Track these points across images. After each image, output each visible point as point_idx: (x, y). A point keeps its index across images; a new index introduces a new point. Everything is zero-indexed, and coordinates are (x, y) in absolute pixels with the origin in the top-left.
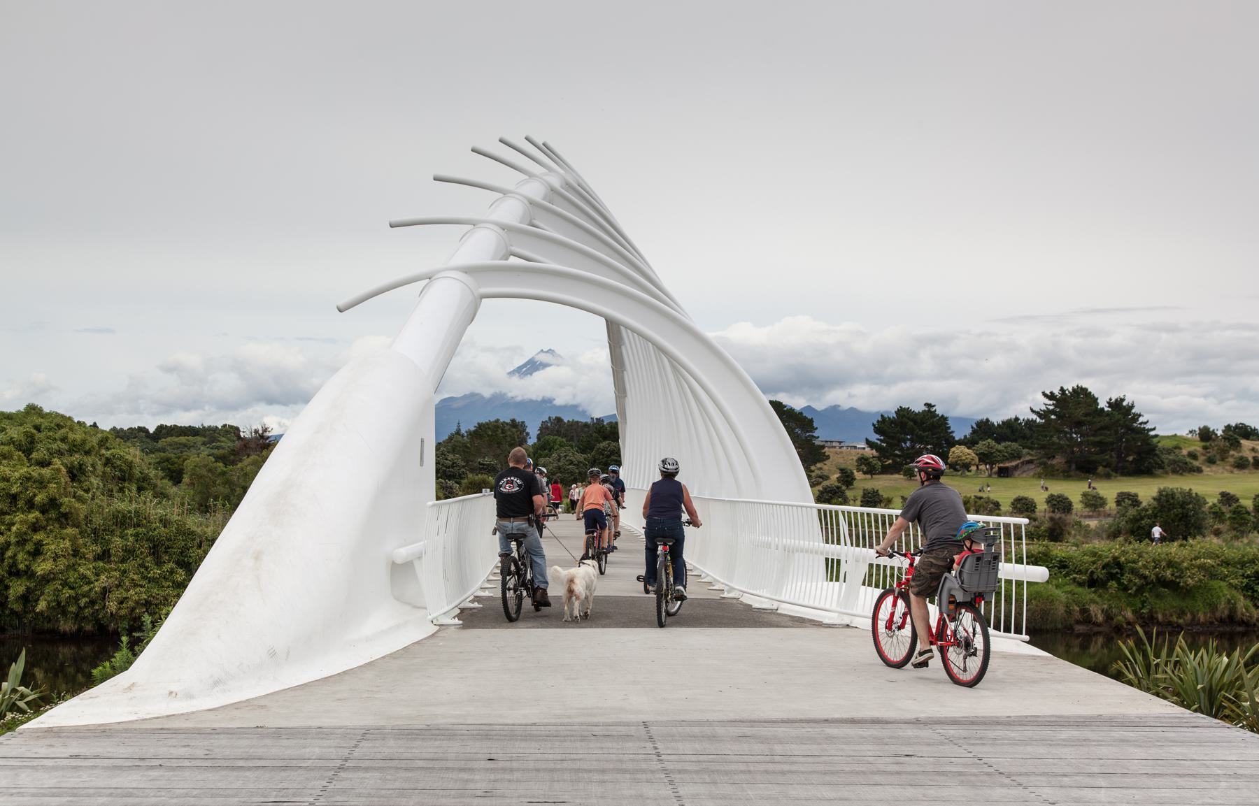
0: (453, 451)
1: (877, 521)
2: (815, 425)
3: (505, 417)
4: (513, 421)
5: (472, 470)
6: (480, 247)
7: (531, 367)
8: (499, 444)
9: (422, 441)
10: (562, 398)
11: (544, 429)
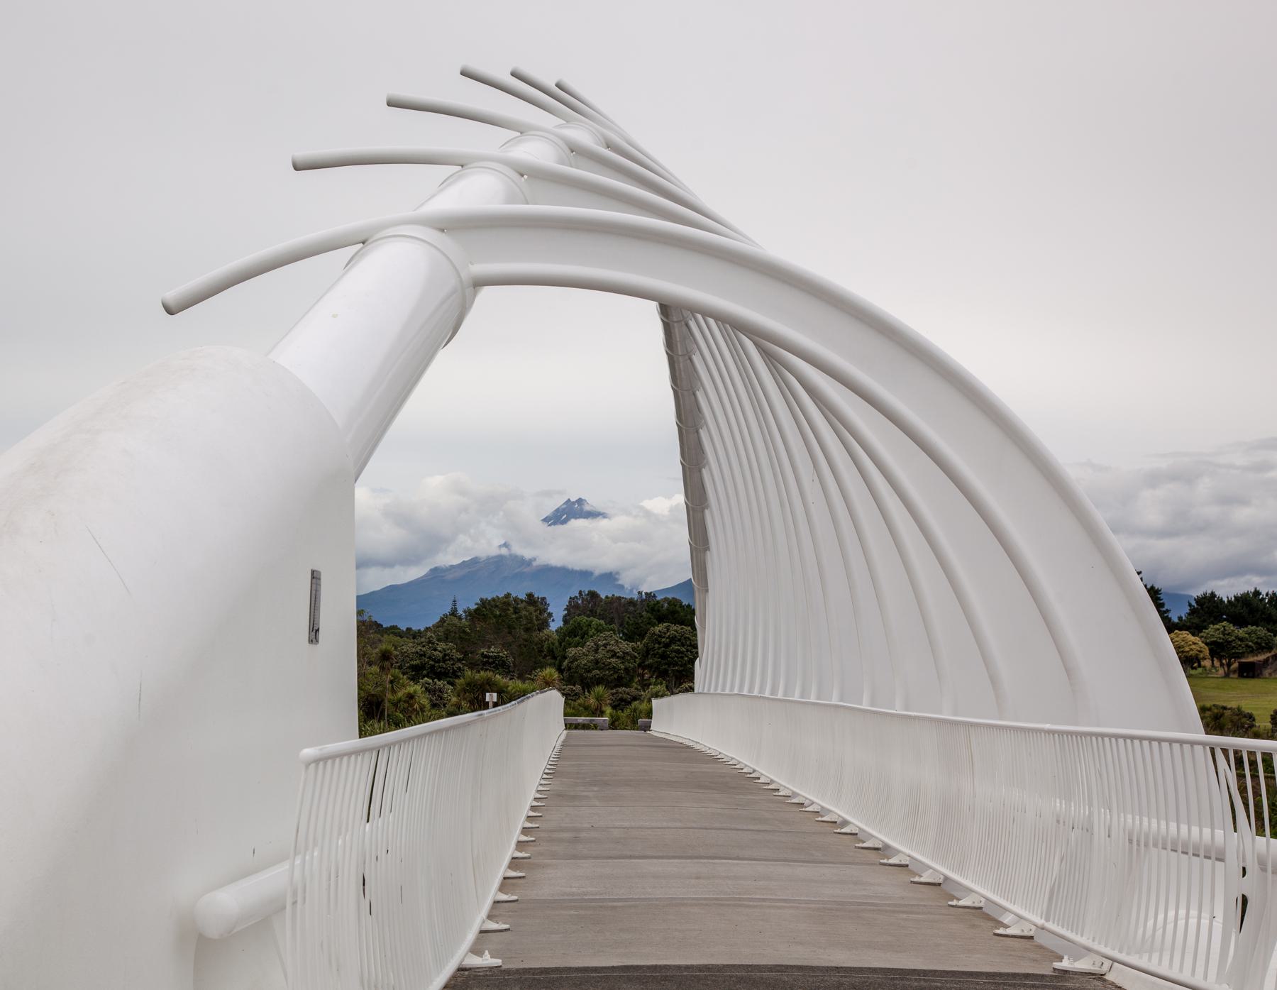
0: (447, 638)
1: (1253, 764)
4: (530, 596)
5: (472, 666)
8: (511, 628)
9: (315, 576)
11: (573, 608)
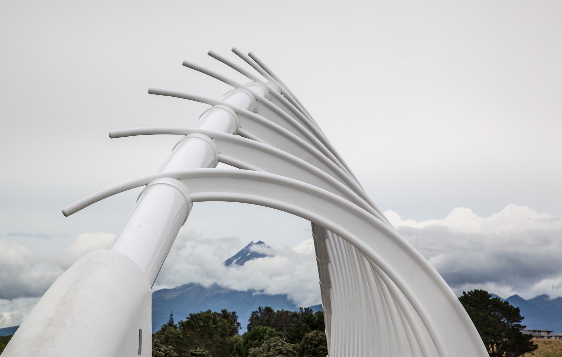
0: (166, 342)
2: (522, 314)
3: (217, 309)
4: (224, 311)
6: (190, 155)
7: (244, 256)
8: (211, 335)
10: (274, 287)
